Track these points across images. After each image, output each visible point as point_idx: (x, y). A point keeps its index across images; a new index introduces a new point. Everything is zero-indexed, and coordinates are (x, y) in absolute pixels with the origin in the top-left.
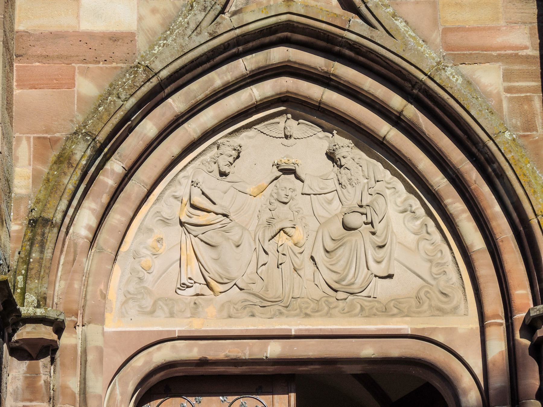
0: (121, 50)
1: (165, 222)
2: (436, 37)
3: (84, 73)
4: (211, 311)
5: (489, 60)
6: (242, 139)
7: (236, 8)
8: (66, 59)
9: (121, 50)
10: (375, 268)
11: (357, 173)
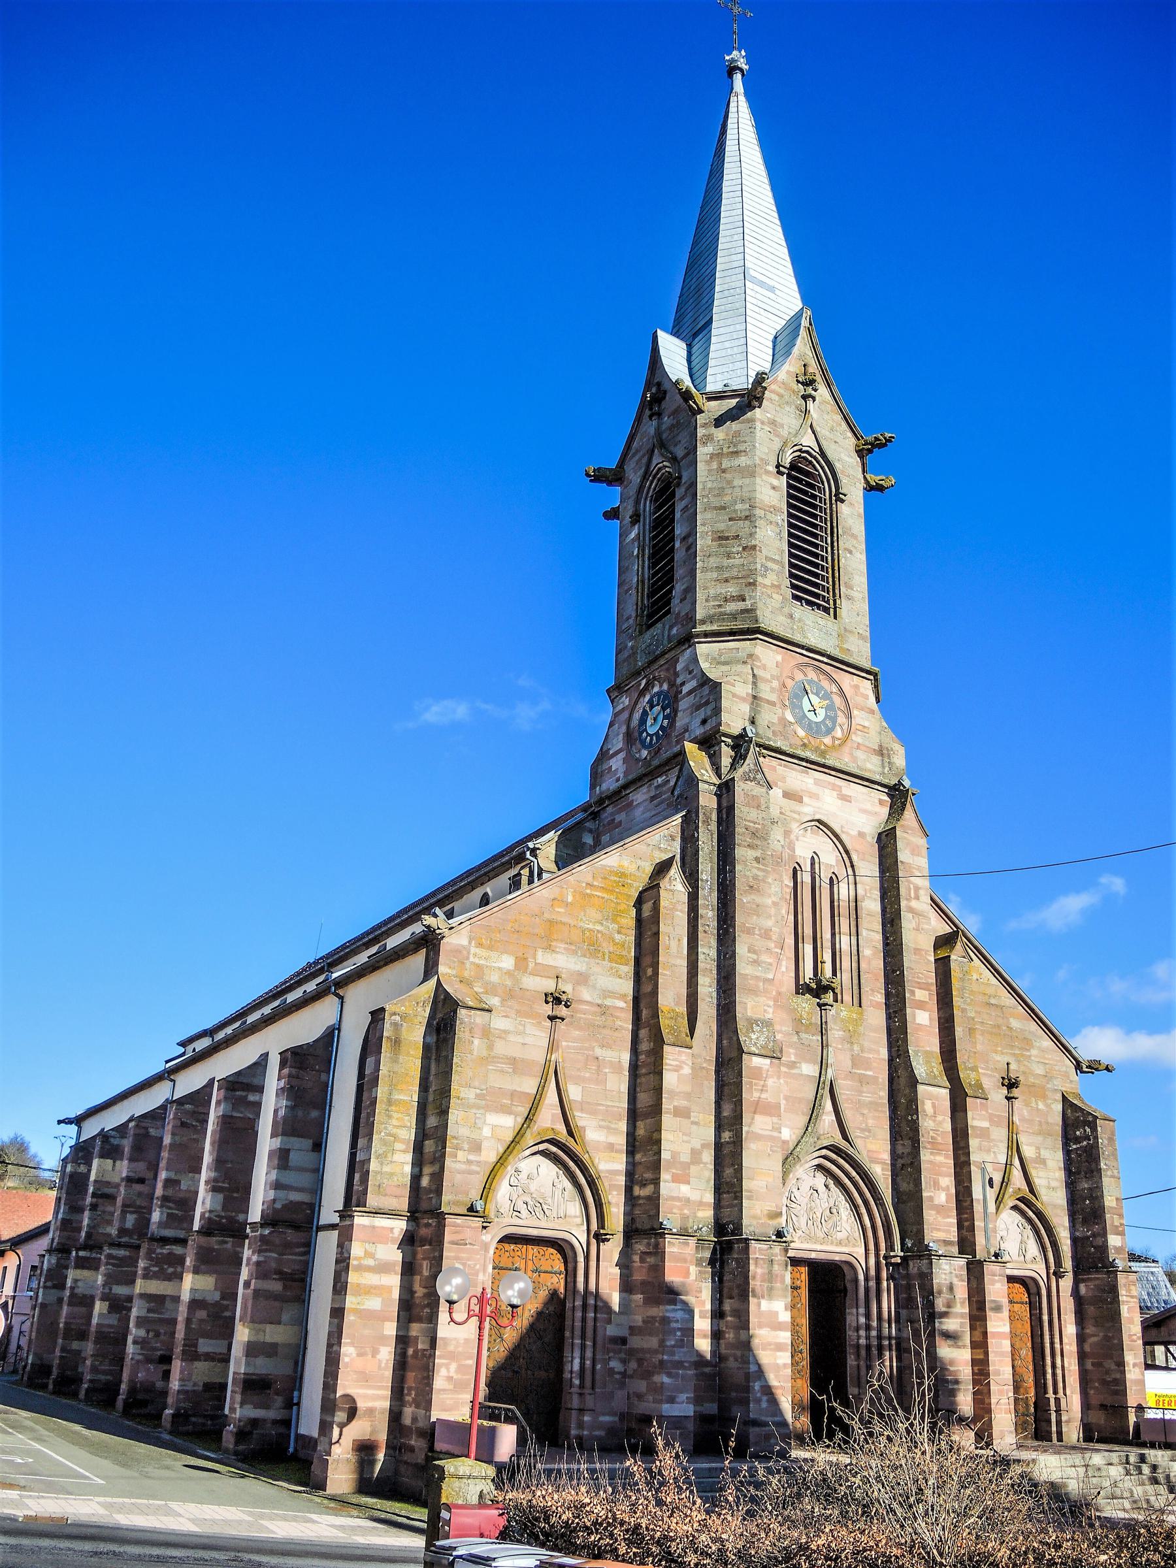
5: (878, 1163)
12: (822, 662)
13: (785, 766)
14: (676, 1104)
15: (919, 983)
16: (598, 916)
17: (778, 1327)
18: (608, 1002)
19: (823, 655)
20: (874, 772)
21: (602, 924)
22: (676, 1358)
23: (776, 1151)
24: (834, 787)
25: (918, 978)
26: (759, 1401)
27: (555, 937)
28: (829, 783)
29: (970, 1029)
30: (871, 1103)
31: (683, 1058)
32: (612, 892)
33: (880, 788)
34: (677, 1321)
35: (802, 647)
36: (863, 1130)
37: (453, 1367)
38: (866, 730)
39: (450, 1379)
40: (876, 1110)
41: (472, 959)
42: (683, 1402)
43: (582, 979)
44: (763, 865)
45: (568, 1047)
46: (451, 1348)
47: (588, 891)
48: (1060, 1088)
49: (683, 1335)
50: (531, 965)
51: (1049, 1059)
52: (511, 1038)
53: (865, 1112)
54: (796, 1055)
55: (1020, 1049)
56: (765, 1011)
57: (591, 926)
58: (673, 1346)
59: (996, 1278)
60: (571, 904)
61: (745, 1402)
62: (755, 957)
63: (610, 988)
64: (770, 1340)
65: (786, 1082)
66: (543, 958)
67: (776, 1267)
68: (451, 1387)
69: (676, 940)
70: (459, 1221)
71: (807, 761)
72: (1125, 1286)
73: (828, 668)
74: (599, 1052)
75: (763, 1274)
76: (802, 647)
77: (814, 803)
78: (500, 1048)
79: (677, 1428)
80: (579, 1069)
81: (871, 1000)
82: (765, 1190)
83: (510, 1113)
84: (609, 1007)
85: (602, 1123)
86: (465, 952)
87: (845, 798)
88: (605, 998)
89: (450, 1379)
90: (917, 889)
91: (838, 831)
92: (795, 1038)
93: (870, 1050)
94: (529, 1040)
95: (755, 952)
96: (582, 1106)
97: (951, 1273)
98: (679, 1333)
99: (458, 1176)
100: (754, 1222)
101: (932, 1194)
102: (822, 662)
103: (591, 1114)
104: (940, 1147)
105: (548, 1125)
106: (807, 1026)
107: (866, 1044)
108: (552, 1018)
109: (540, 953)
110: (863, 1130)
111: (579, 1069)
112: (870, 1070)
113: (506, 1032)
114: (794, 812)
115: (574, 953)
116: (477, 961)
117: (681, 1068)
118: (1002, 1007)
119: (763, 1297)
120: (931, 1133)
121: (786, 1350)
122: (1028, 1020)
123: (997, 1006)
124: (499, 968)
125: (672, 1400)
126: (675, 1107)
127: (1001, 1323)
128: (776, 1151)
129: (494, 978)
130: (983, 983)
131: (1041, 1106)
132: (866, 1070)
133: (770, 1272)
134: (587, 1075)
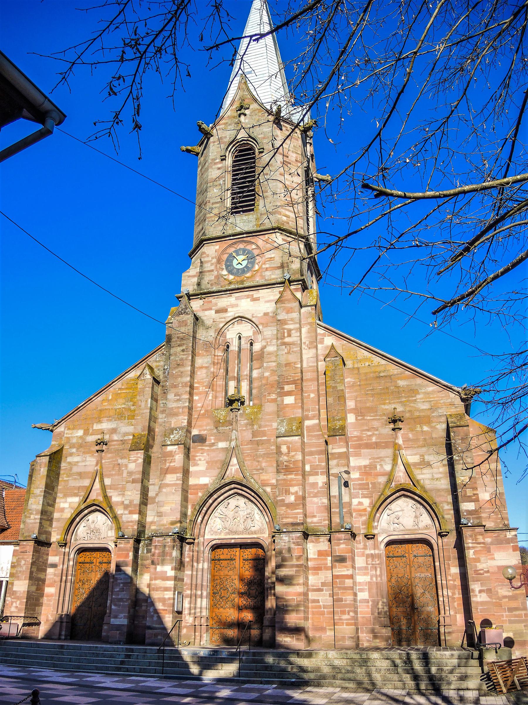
0: (206, 487)
1: (216, 517)
2: (260, 482)
3: (200, 492)
4: (223, 534)
5: (268, 486)
6: (229, 501)
7: (506, 534)
8: (197, 489)
9: (206, 487)
10: (252, 525)
11: (249, 506)
12: (243, 237)
13: (217, 298)
14: (133, 477)
15: (287, 382)
16: (124, 401)
17: (168, 579)
18: (126, 438)
19: (243, 234)
20: (277, 279)
21: (125, 404)
22: (120, 597)
23: (178, 491)
24: (248, 297)
25: (287, 379)
26: (152, 617)
27: (102, 416)
28: (245, 296)
29: (339, 397)
30: (264, 454)
31: (139, 455)
32: (130, 388)
33: (279, 286)
34: (121, 579)
35: (230, 236)
36: (257, 470)
37: (18, 602)
38: (272, 259)
39: (17, 607)
40: (268, 457)
41: (65, 436)
42: (121, 618)
43: (114, 431)
44: (186, 352)
45: (105, 462)
46: (18, 595)
47: (119, 392)
48: (445, 413)
49: (124, 586)
50: (91, 431)
51: (432, 398)
52: (80, 464)
53: (261, 459)
54: (214, 439)
55: (406, 397)
56: (182, 422)
57: (120, 407)
58: (117, 591)
59: (342, 541)
60: (111, 400)
61: (144, 617)
62: (178, 397)
63: (127, 432)
64: (161, 585)
65: (208, 455)
66: (96, 427)
67: (167, 549)
68: (17, 610)
69: (145, 401)
70: (25, 543)
71: (229, 290)
72: (471, 536)
73: (248, 239)
74: (120, 461)
75: (159, 553)
76: (230, 236)
77: (235, 309)
78: (75, 469)
79: (117, 630)
80: (110, 471)
81: (268, 399)
82: (170, 511)
83: (77, 496)
84: (126, 440)
85: (120, 493)
86: (62, 434)
87: (255, 300)
88: (125, 436)
89: (17, 607)
90: (289, 331)
91: (250, 317)
92: (215, 431)
93: (266, 426)
94: (87, 463)
95: (179, 395)
96: (111, 487)
97: (289, 541)
98: (121, 585)
99: (31, 525)
100: (162, 528)
101: (284, 498)
102: (243, 237)
103: (115, 489)
104: (292, 470)
105: (94, 498)
106: (223, 423)
107: (263, 423)
108: (394, 429)
109: (95, 425)
110: (257, 470)
111: (110, 471)
112: (265, 436)
113: (77, 462)
114: (222, 318)
115: (111, 420)
116: (67, 436)
117: (137, 460)
118: (390, 376)
119: (158, 564)
120: (285, 463)
121: (170, 591)
122: (414, 378)
123: (386, 376)
124: (77, 436)
125: (116, 617)
126: (133, 479)
127: (345, 569)
128: (178, 491)
129: (74, 441)
130: (374, 366)
131: (425, 428)
132: (262, 437)
133: (163, 552)
134: (114, 473)
